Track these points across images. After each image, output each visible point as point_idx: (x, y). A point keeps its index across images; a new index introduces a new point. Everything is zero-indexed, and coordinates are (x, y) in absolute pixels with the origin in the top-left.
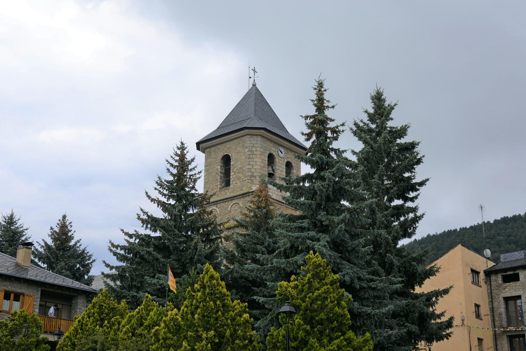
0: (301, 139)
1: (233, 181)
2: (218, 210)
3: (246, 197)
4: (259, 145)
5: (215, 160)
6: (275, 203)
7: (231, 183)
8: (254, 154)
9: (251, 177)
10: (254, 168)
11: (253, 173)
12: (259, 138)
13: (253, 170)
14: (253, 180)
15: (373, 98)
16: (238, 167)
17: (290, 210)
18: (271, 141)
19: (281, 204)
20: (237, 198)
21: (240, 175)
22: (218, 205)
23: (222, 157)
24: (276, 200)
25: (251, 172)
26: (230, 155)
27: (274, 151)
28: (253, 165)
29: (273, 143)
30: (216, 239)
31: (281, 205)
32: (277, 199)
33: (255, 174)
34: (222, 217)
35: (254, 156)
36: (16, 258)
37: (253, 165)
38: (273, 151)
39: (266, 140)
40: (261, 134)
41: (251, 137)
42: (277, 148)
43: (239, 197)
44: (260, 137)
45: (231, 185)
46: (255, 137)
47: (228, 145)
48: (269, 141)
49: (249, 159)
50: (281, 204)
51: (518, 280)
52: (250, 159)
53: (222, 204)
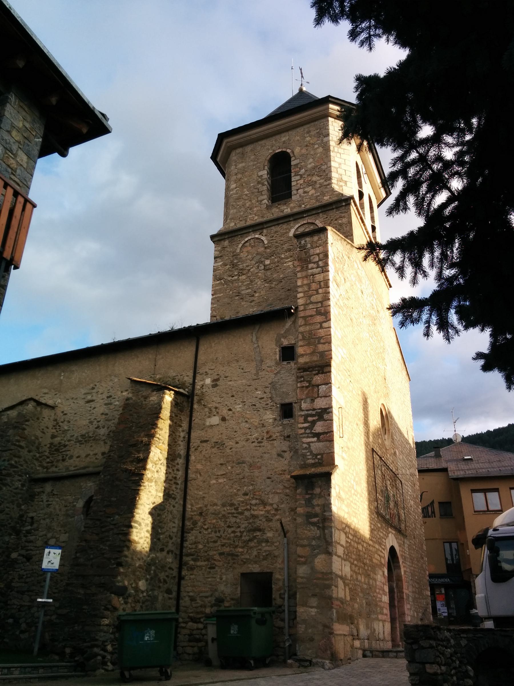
0: (386, 175)
1: (297, 190)
2: (263, 238)
3: (330, 212)
5: (256, 163)
7: (294, 192)
11: (341, 175)
14: (342, 186)
15: (417, 283)
16: (309, 166)
20: (310, 214)
21: (315, 178)
22: (265, 231)
23: (270, 156)
26: (289, 151)
30: (39, 493)
32: (192, 441)
34: (274, 249)
43: (314, 212)
45: (293, 197)
47: (284, 138)
53: (273, 228)
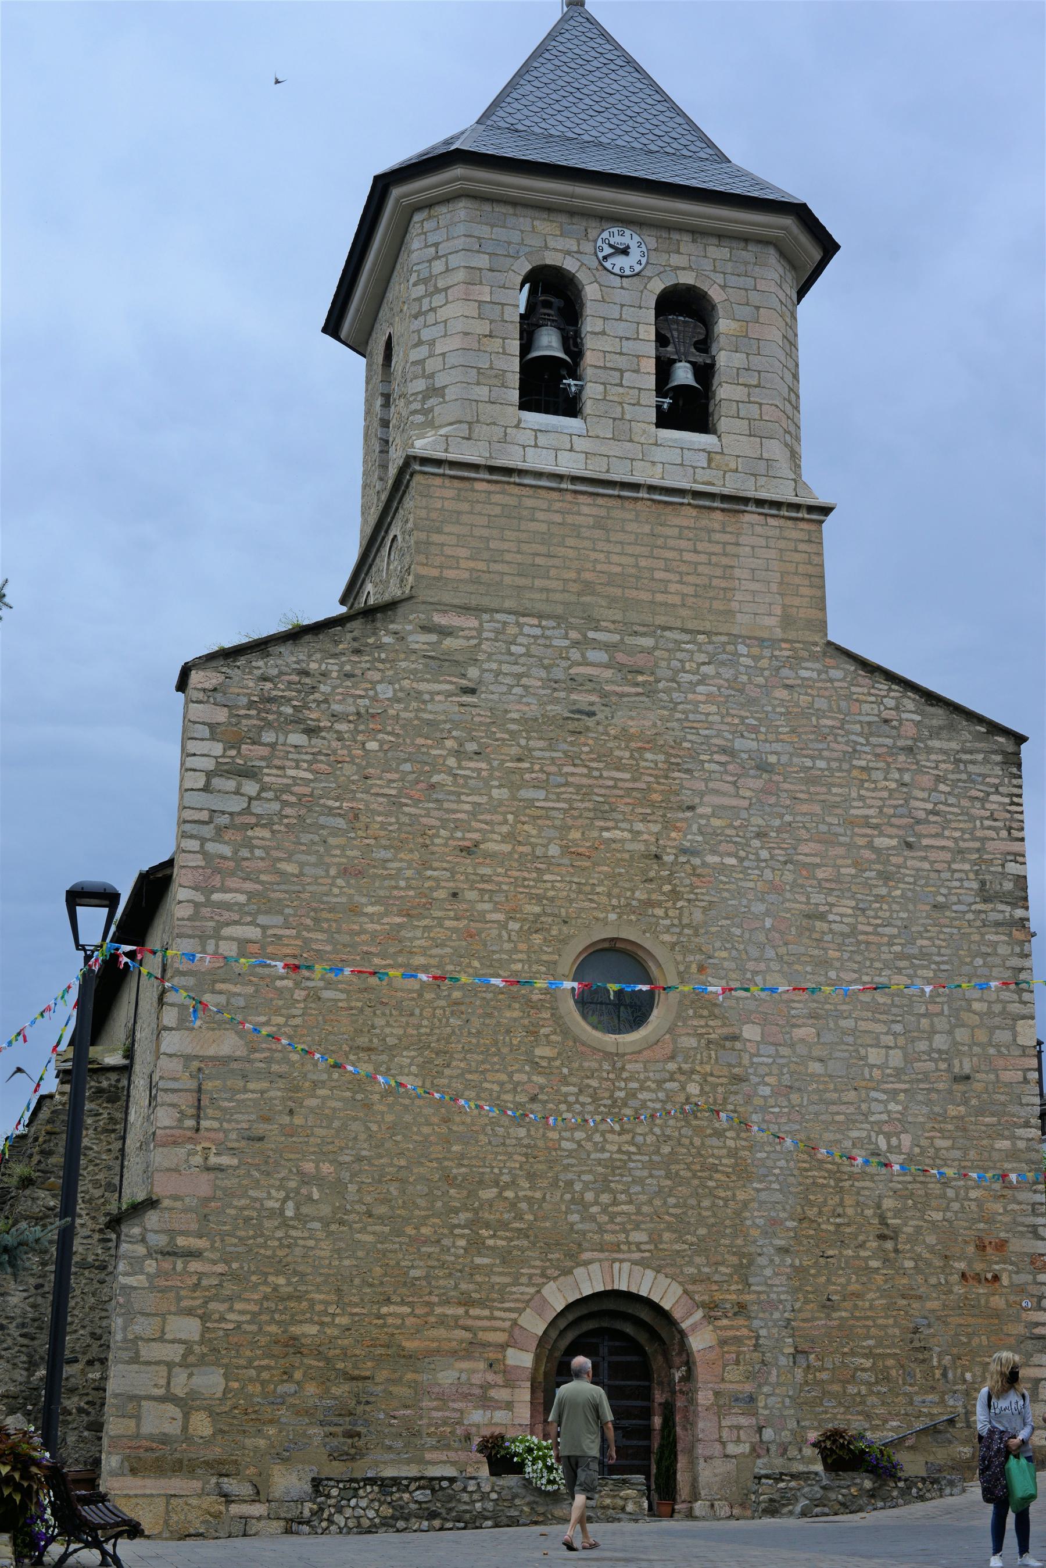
4: (459, 243)
6: (575, 492)
8: (438, 291)
9: (425, 398)
10: (437, 352)
11: (432, 376)
12: (462, 210)
13: (431, 365)
14: (431, 410)
17: (694, 512)
18: (548, 209)
19: (616, 493)
24: (575, 479)
25: (424, 376)
27: (568, 253)
28: (432, 343)
29: (563, 218)
31: (619, 496)
33: (440, 381)
35: (438, 300)
36: (1027, 908)
37: (432, 343)
38: (560, 255)
39: (510, 210)
40: (457, 186)
41: (430, 217)
42: (592, 233)
44: (462, 203)
46: (443, 209)
48: (530, 212)
49: (416, 317)
50: (616, 493)
51: (526, 405)
52: (421, 319)
